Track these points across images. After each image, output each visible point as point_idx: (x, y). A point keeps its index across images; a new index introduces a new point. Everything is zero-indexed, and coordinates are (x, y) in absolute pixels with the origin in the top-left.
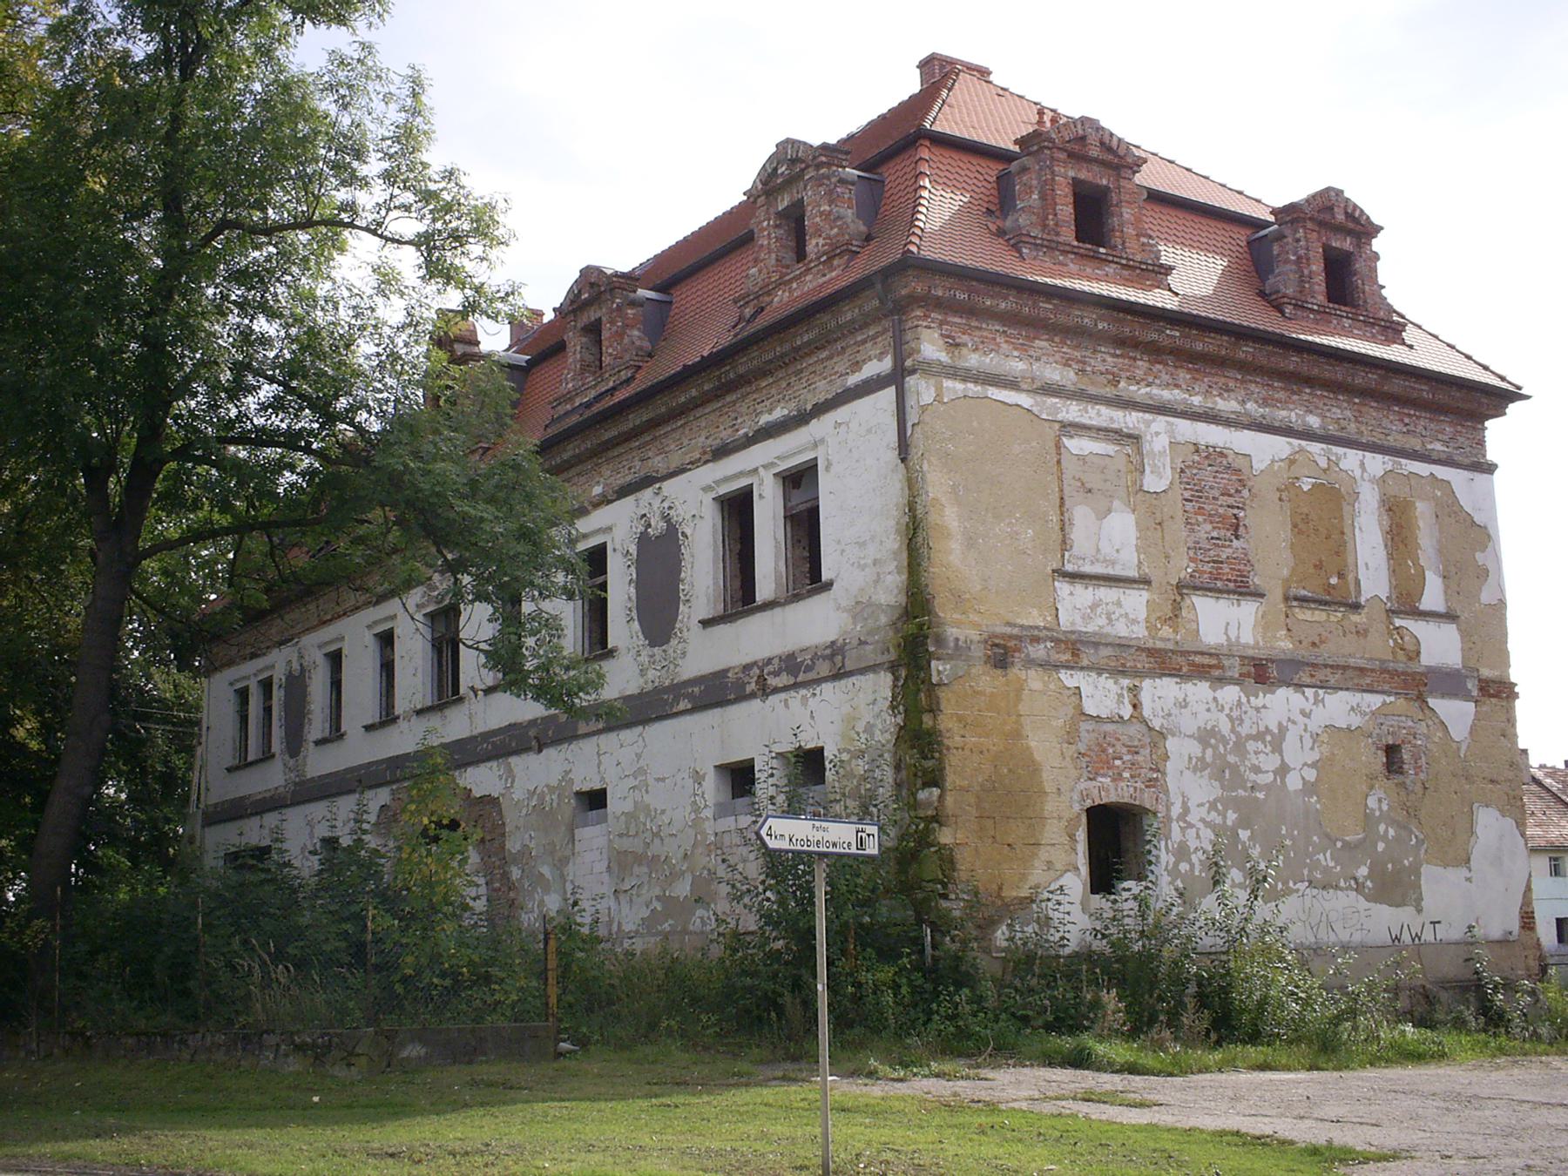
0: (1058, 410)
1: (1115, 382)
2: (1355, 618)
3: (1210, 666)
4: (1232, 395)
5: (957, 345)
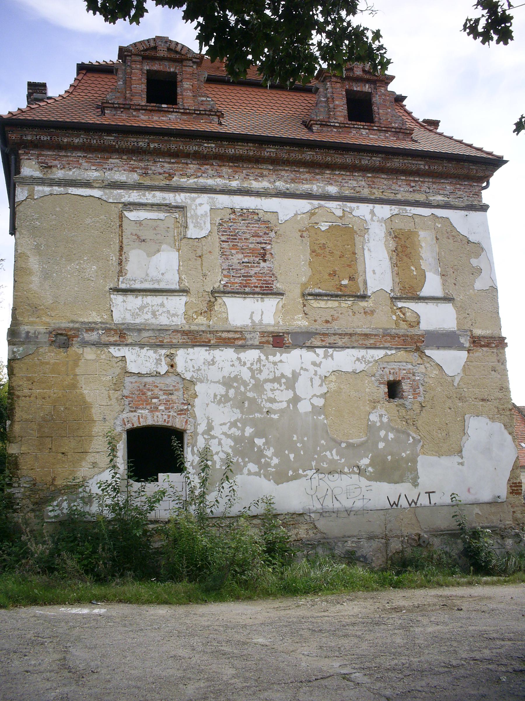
0: (121, 196)
1: (171, 176)
2: (363, 304)
3: (235, 339)
4: (265, 179)
5: (50, 167)
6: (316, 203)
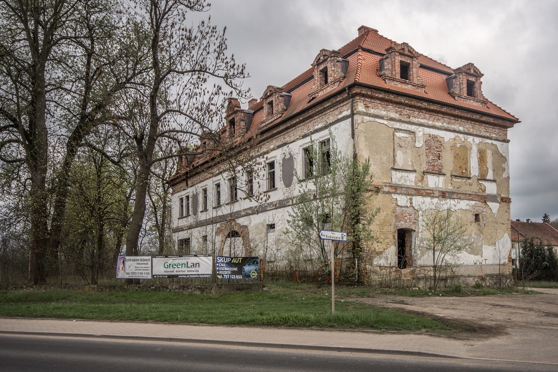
0: (394, 125)
2: (469, 181)
6: (456, 134)
